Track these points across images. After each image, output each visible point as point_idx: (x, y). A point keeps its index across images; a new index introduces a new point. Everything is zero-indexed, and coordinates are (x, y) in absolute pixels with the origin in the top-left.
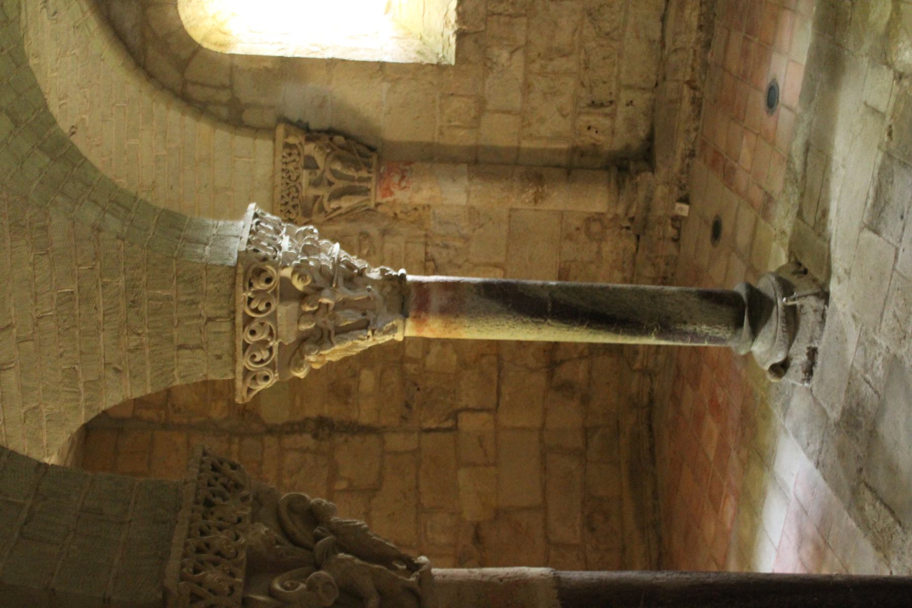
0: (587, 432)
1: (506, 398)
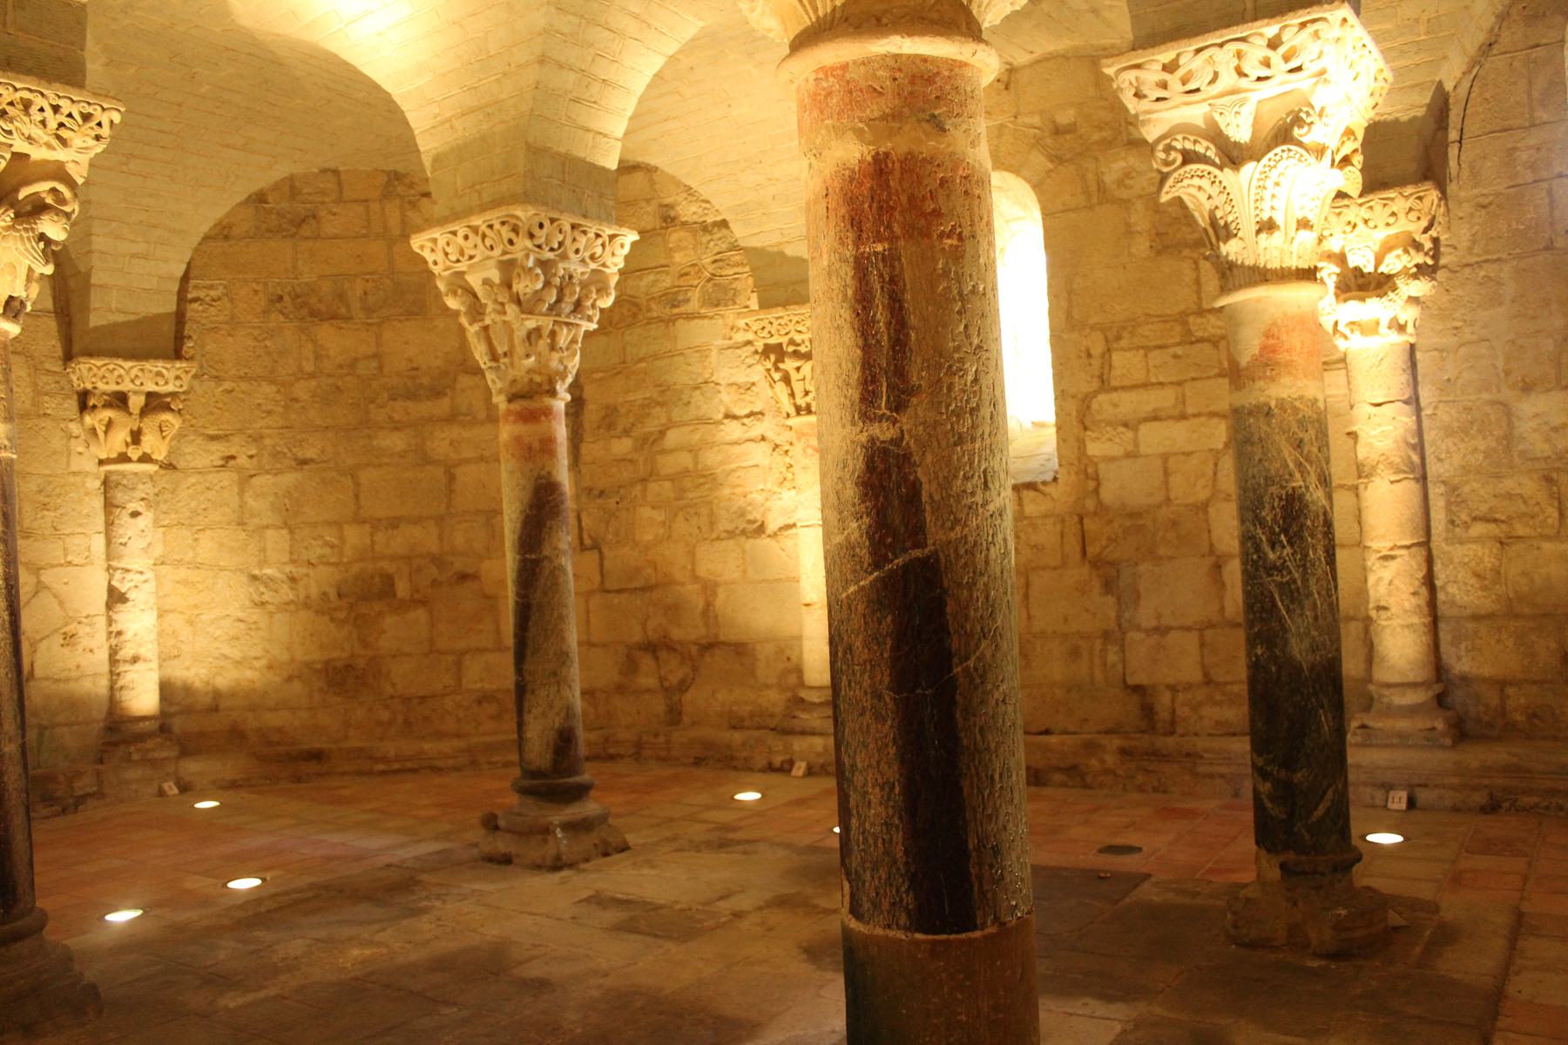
1: (616, 600)
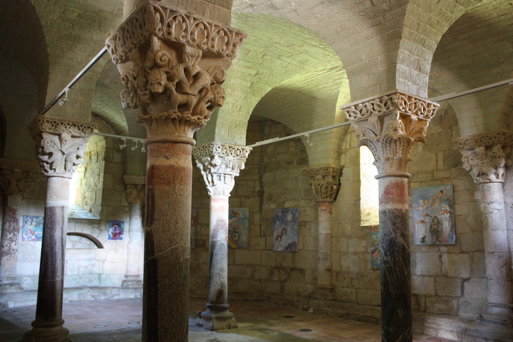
0: (260, 280)
